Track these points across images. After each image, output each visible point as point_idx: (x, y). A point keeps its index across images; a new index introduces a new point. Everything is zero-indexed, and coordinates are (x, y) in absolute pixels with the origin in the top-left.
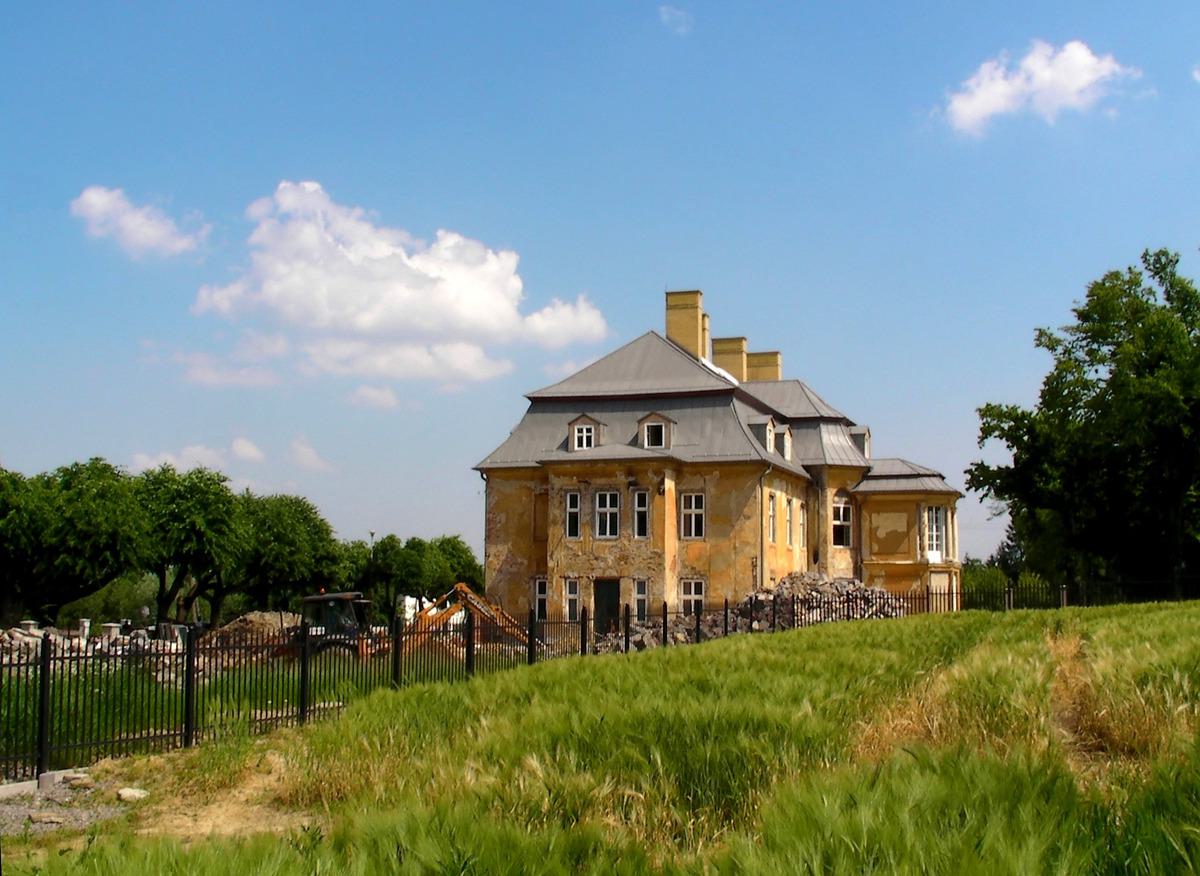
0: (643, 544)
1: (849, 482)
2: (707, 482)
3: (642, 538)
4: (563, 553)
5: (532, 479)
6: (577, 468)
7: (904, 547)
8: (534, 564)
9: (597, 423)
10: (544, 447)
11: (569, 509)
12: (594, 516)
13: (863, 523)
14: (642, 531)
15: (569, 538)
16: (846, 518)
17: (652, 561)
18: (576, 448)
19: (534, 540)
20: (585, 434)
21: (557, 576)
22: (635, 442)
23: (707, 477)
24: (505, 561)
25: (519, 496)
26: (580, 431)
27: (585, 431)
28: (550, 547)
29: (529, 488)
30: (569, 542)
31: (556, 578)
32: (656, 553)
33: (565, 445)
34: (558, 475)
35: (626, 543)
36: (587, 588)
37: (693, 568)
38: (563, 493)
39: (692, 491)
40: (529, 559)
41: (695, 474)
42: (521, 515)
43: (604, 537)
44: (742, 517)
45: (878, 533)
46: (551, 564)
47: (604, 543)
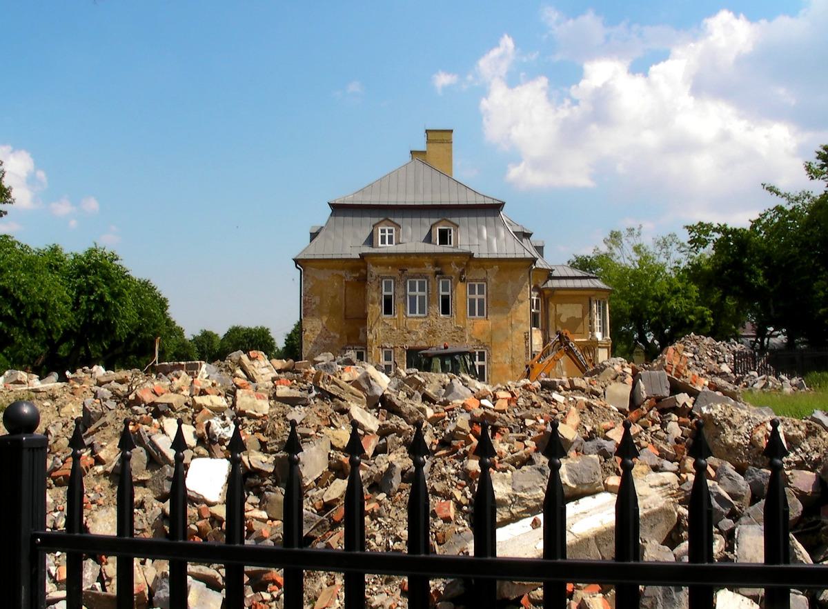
0: (448, 321)
1: (540, 281)
2: (488, 274)
3: (446, 316)
4: (380, 328)
5: (343, 269)
6: (393, 259)
7: (580, 329)
8: (345, 337)
9: (398, 226)
10: (349, 242)
11: (384, 293)
12: (406, 299)
13: (550, 311)
14: (445, 310)
15: (384, 316)
16: (537, 308)
17: (455, 334)
18: (380, 245)
19: (346, 319)
20: (387, 234)
21: (376, 346)
22: (429, 239)
23: (488, 270)
24: (319, 335)
25: (333, 285)
26: (383, 231)
27: (387, 231)
28: (369, 323)
29: (340, 276)
30: (386, 319)
31: (374, 348)
32: (459, 328)
33: (370, 241)
34: (376, 265)
35: (434, 319)
36: (401, 355)
37: (478, 341)
38: (380, 279)
39: (476, 280)
40: (341, 334)
41: (480, 267)
42: (334, 298)
43: (414, 315)
44: (517, 302)
45: (561, 319)
46: (370, 337)
47: (415, 320)
